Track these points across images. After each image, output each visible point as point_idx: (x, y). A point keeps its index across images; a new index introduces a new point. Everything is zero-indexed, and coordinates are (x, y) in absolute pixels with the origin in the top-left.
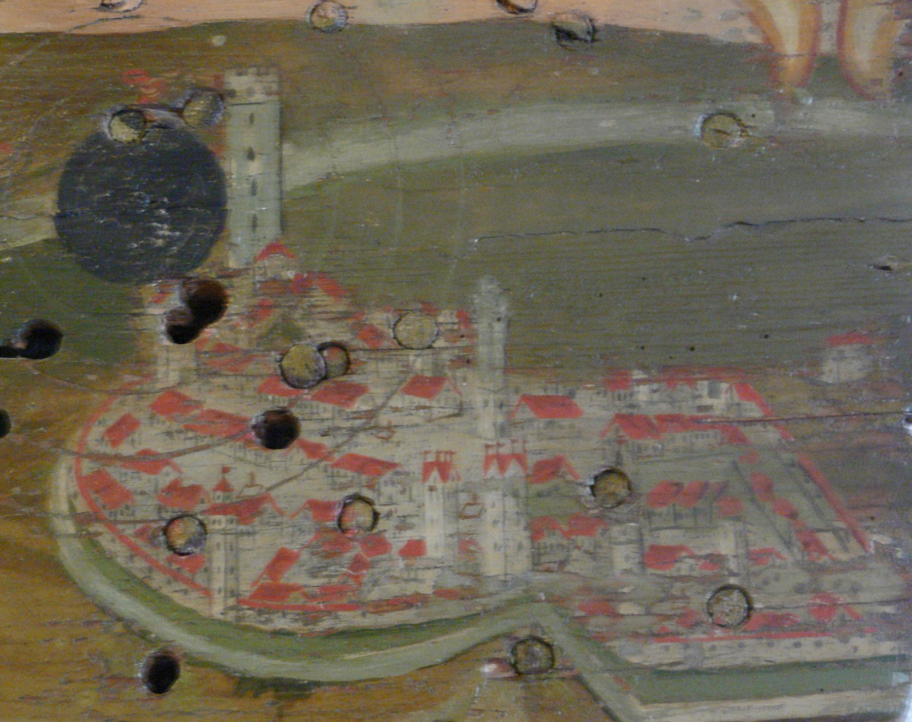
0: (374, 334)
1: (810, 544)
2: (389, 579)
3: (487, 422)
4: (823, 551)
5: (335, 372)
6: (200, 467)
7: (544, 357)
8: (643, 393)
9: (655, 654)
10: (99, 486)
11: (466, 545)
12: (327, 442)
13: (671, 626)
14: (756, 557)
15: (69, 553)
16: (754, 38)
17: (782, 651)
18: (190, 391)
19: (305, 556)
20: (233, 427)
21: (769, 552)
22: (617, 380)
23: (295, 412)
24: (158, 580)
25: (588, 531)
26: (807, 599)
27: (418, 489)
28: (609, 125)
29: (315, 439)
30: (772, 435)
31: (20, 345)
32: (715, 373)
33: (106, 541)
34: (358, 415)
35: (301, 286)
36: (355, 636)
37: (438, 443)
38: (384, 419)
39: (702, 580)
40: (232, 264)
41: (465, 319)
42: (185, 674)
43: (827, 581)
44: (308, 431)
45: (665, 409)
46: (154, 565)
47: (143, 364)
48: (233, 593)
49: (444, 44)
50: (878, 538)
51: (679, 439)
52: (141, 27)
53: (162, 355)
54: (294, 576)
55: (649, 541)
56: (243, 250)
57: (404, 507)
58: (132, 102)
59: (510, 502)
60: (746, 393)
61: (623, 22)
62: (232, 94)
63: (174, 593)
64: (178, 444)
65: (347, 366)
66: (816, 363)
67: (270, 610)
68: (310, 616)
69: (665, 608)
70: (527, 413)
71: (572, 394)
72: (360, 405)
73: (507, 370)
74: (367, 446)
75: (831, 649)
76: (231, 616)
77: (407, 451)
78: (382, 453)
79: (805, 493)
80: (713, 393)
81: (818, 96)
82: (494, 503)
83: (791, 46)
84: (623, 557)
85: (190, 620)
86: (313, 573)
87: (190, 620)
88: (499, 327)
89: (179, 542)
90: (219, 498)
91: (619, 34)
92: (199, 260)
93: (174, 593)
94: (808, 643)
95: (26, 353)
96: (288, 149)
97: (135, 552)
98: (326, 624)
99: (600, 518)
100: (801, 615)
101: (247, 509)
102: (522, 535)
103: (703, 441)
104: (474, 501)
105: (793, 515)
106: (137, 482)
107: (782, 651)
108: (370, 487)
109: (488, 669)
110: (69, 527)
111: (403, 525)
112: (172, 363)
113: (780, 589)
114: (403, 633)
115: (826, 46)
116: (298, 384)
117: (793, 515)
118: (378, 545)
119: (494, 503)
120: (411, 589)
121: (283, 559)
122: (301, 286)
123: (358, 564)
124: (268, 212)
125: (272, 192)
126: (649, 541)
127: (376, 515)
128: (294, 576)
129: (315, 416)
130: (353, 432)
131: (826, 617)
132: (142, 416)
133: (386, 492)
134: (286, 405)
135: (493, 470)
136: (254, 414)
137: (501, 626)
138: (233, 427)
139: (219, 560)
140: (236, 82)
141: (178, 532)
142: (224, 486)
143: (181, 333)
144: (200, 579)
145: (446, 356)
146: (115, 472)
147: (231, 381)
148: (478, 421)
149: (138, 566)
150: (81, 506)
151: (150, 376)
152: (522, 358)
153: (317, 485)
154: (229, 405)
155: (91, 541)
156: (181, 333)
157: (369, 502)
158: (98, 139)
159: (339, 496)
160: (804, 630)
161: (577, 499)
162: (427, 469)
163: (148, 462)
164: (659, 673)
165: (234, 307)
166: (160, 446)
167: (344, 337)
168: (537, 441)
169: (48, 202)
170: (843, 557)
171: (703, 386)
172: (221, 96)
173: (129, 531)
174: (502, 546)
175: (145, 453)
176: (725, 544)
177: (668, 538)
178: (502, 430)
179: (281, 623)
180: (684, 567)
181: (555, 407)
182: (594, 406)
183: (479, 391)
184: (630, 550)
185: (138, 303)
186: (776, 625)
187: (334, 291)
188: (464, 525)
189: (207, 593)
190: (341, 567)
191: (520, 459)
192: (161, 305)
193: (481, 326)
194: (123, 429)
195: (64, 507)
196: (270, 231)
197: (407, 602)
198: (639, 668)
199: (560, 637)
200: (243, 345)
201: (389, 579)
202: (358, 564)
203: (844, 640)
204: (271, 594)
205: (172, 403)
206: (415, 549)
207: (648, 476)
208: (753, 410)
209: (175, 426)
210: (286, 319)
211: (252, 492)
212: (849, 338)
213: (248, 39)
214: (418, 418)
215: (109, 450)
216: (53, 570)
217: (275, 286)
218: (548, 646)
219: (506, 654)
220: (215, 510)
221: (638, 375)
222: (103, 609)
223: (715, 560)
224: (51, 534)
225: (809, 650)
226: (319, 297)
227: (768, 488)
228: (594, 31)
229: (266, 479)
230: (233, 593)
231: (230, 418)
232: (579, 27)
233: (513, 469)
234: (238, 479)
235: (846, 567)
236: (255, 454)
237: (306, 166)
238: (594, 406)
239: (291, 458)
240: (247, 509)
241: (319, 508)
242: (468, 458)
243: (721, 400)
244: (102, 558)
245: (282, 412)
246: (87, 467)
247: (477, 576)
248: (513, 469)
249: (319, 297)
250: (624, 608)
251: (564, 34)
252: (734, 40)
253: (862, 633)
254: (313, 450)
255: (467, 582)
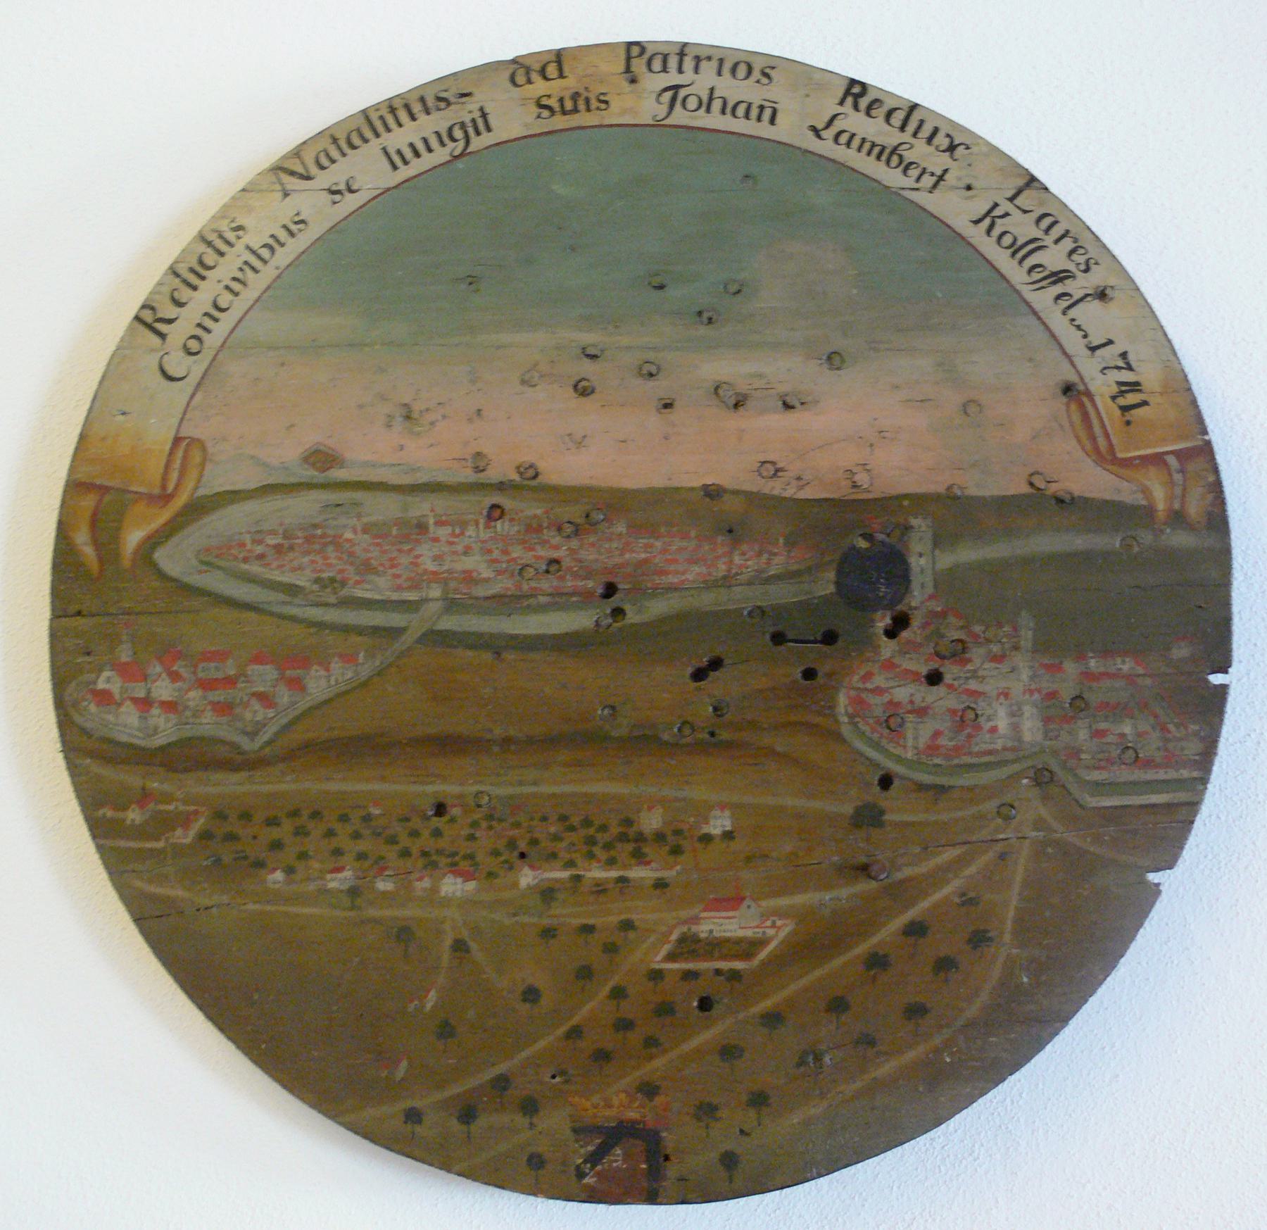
0: (976, 636)
1: (1164, 729)
2: (983, 742)
3: (1025, 675)
4: (1169, 732)
5: (959, 653)
6: (902, 694)
7: (1050, 648)
8: (1093, 663)
9: (1096, 776)
10: (858, 702)
11: (1015, 727)
12: (956, 683)
13: (1103, 764)
14: (1140, 735)
15: (846, 730)
16: (1144, 503)
17: (1150, 775)
18: (896, 661)
19: (946, 732)
20: (915, 676)
21: (1146, 733)
22: (1081, 657)
23: (942, 670)
24: (884, 742)
25: (1068, 722)
26: (1162, 753)
27: (994, 704)
28: (1080, 542)
29: (951, 682)
30: (1148, 681)
31: (819, 638)
32: (1125, 653)
33: (861, 726)
34: (969, 671)
35: (943, 614)
36: (970, 767)
37: (1003, 684)
38: (980, 673)
39: (1117, 744)
40: (913, 604)
41: (1015, 629)
42: (896, 783)
43: (1170, 746)
44: (948, 678)
45: (1102, 669)
46: (882, 736)
47: (876, 649)
48: (916, 748)
49: (1004, 505)
50: (1194, 727)
51: (1107, 683)
52: (871, 496)
53: (882, 644)
54: (943, 741)
55: (1094, 727)
56: (918, 597)
57: (989, 712)
58: (868, 531)
59: (1035, 711)
60: (1138, 663)
61: (1087, 495)
62: (912, 527)
63: (891, 748)
64: (892, 684)
65: (964, 650)
66: (1169, 649)
67: (931, 755)
68: (948, 757)
69: (1100, 756)
70: (1043, 671)
71: (1061, 663)
72: (969, 667)
73: (1035, 651)
74: (973, 685)
75: (1171, 774)
76: (915, 758)
77: (990, 687)
78: (980, 688)
79: (1163, 707)
80: (1124, 662)
81: (1173, 529)
82: (1028, 710)
83: (1161, 506)
84: (1083, 734)
85: (899, 759)
86: (951, 739)
87: (899, 759)
88: (1030, 633)
89: (892, 726)
90: (909, 707)
91: (1086, 500)
92: (900, 601)
93: (891, 748)
94: (1162, 772)
95: (822, 642)
96: (937, 552)
97: (873, 730)
98: (956, 761)
99: (1072, 718)
100: (1158, 760)
101: (922, 712)
102: (1040, 724)
103: (1119, 684)
104: (1020, 709)
105: (1156, 716)
106: (874, 700)
107: (1150, 775)
108: (976, 703)
109: (1025, 781)
110: (846, 719)
111: (989, 719)
112: (888, 648)
113: (1151, 747)
114: (988, 766)
115: (1177, 506)
116: (943, 658)
117: (1156, 716)
118: (979, 728)
119: (1028, 710)
120: (991, 747)
121: (937, 734)
122: (943, 614)
123: (970, 736)
124: (929, 580)
125: (929, 572)
126: (1094, 727)
127: (977, 715)
128: (943, 741)
129: (951, 672)
130: (967, 678)
131: (1170, 760)
132: (876, 671)
133: (981, 705)
134: (473, 1127)
135: (1027, 696)
136: (924, 670)
137: (1030, 763)
138: (915, 676)
139: (910, 734)
140: (914, 522)
141: (892, 723)
142: (911, 702)
143: (891, 633)
144: (901, 742)
145: (1007, 646)
146: (864, 695)
147: (914, 656)
148: (1021, 675)
149: (876, 736)
150: (850, 710)
151: (879, 654)
152: (1041, 647)
153: (952, 702)
154: (912, 666)
155: (855, 725)
156: (891, 633)
157: (973, 709)
158: (853, 548)
159: (962, 706)
160: (1158, 766)
161: (1063, 708)
162: (999, 695)
163: (878, 691)
164: (1097, 784)
165: (916, 623)
166: (883, 684)
167: (963, 637)
168: (1047, 684)
169: (831, 575)
170: (1178, 735)
171: (1119, 660)
172: (908, 528)
173: (871, 721)
174: (1031, 728)
175: (877, 687)
176: (1127, 729)
177: (1103, 726)
178: (1032, 678)
179: (937, 761)
180: (1110, 738)
181: (1055, 668)
182: (1071, 668)
183: (1022, 662)
184: (1086, 731)
185: (873, 621)
186: (1149, 764)
187: (959, 616)
188: (1015, 719)
189: (905, 747)
190: (962, 737)
191: (1039, 691)
192: (883, 621)
193: (1023, 633)
194: (868, 676)
195: (843, 711)
196: (930, 590)
197: (990, 753)
198: (1088, 782)
199: (1055, 768)
200: (919, 640)
201: (983, 742)
202: (970, 736)
203: (1177, 771)
204: (932, 749)
205: (889, 665)
206: (994, 730)
207: (1094, 698)
208: (1140, 670)
209: (890, 676)
210: (938, 629)
211: (923, 705)
212: (1184, 638)
213: (920, 502)
214: (995, 673)
215: (861, 685)
216: (839, 737)
217: (934, 614)
218: (1051, 772)
219: (1032, 775)
220: (909, 712)
221: (1091, 655)
222: (861, 754)
223: (1123, 735)
224: (837, 721)
225: (1161, 775)
226: (952, 619)
227: (1146, 705)
228: (1073, 499)
229: (930, 699)
230: (916, 748)
231: (912, 672)
232: (1067, 498)
233: (1036, 696)
234: (917, 699)
235: (1181, 739)
236: (924, 688)
237: (946, 560)
238: (1071, 668)
239: (940, 690)
240: (922, 712)
241: (953, 712)
242: (1017, 688)
243: (1127, 665)
244: (862, 734)
245: (937, 670)
246: (853, 693)
247: (1020, 740)
248: (1036, 696)
249: (952, 619)
250: (1083, 756)
251: (1060, 501)
252: (1136, 503)
253: (1185, 768)
254: (950, 686)
255: (1016, 744)
